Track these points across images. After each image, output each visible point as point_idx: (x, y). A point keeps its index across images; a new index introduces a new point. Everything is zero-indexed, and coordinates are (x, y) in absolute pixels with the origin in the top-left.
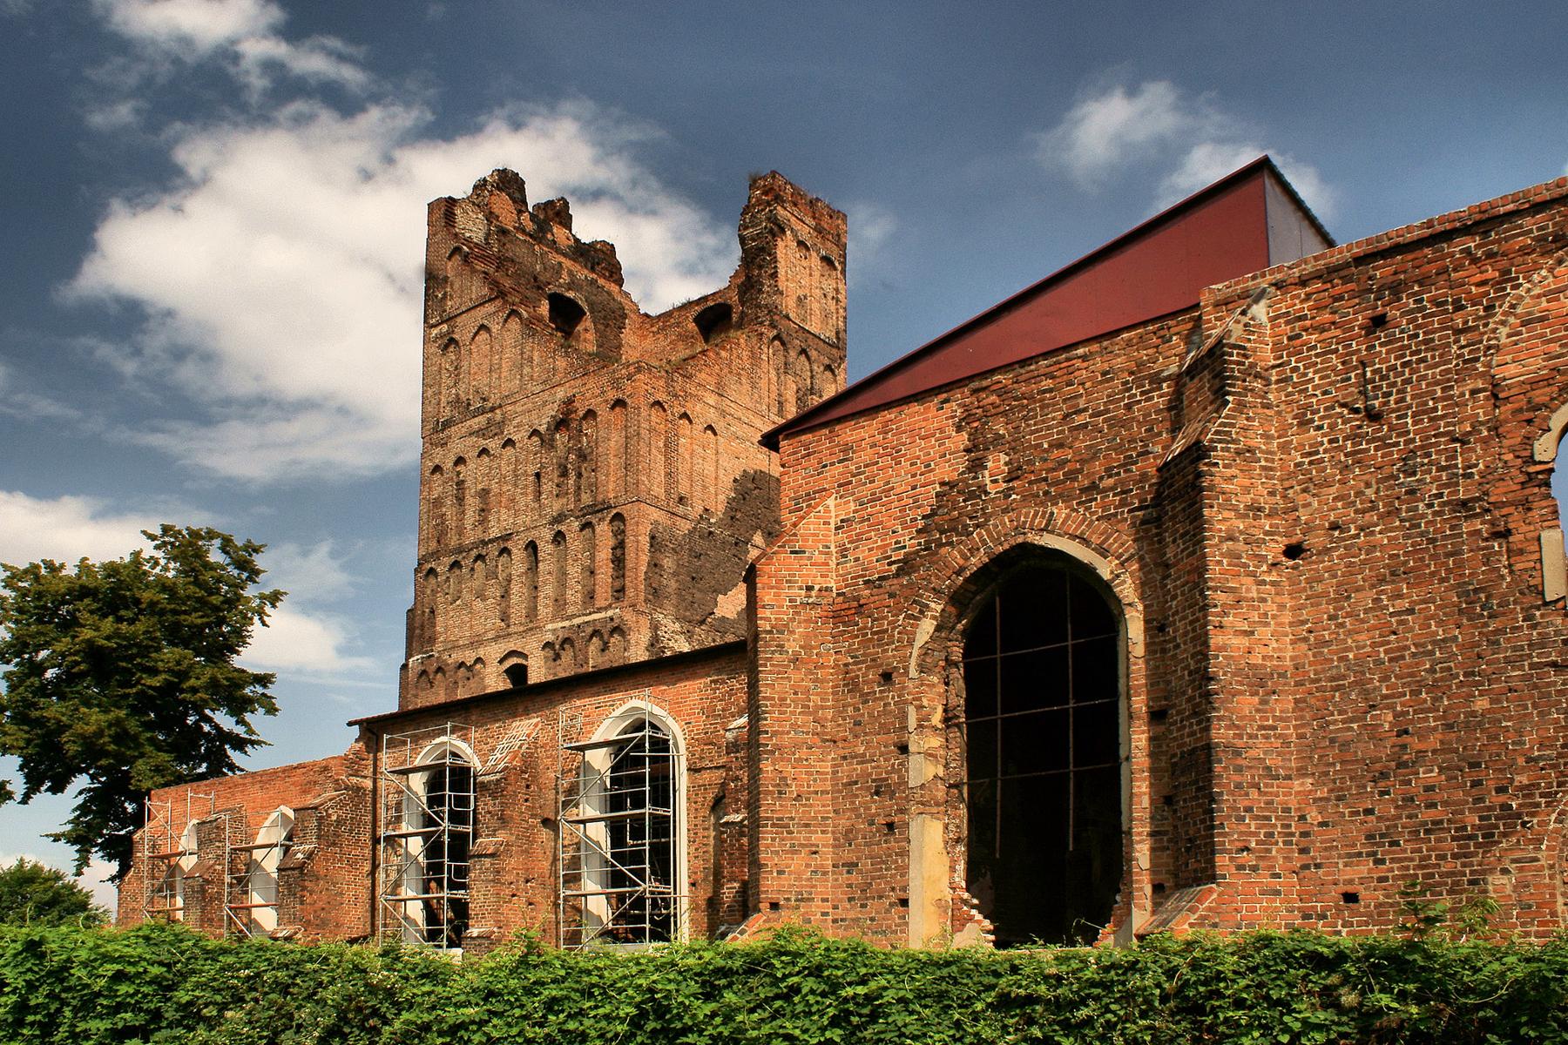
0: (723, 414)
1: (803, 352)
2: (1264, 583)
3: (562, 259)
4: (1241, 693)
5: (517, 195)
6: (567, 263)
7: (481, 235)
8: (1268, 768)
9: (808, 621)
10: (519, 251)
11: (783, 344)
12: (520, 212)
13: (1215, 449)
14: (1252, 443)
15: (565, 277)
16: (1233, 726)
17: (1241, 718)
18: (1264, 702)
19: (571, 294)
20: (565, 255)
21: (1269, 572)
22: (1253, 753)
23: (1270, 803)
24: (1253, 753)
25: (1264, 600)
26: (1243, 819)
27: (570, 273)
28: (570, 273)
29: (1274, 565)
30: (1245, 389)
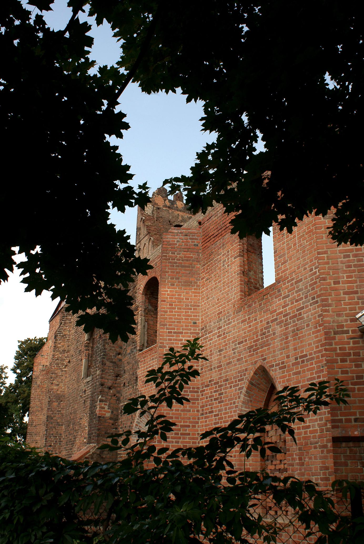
2: (63, 371)
3: (179, 213)
4: (55, 401)
6: (181, 213)
7: (151, 212)
8: (58, 422)
9: (42, 375)
10: (164, 214)
12: (165, 200)
13: (57, 336)
14: (66, 333)
15: (180, 218)
16: (52, 411)
17: (54, 408)
18: (59, 404)
20: (180, 211)
21: (65, 368)
22: (55, 418)
23: (57, 432)
24: (55, 418)
25: (62, 376)
26: (51, 437)
27: (182, 217)
28: (182, 217)
29: (66, 365)
30: (66, 319)
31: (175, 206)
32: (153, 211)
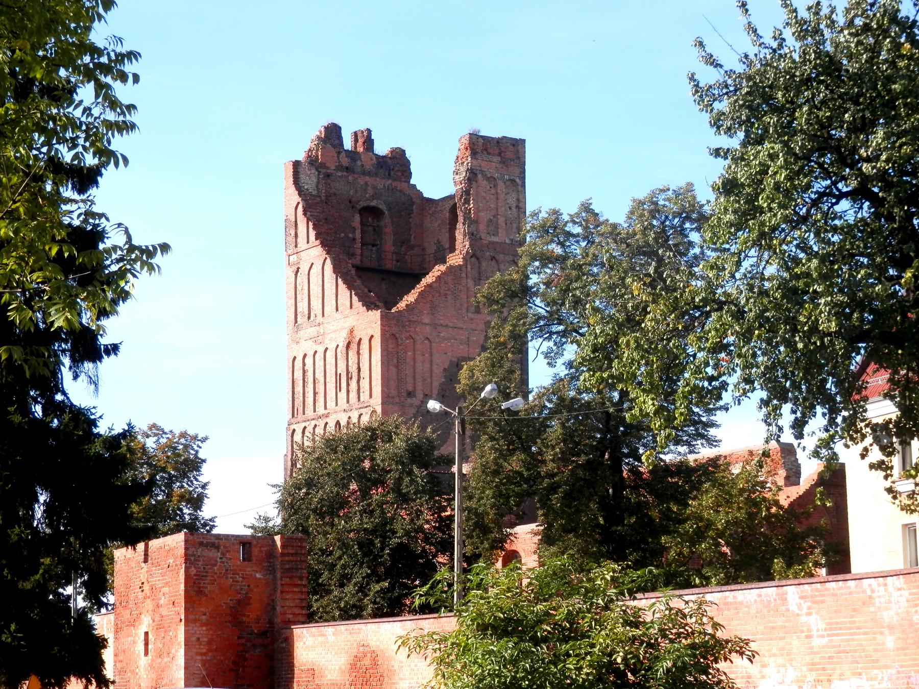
0: (434, 325)
1: (493, 258)
5: (337, 142)
11: (478, 259)
12: (339, 153)
15: (370, 191)
19: (373, 203)
20: (369, 174)
28: (374, 188)
31: (359, 163)
32: (318, 183)
